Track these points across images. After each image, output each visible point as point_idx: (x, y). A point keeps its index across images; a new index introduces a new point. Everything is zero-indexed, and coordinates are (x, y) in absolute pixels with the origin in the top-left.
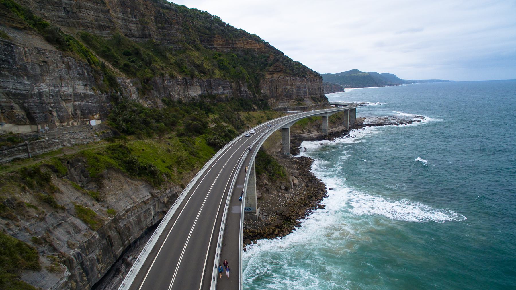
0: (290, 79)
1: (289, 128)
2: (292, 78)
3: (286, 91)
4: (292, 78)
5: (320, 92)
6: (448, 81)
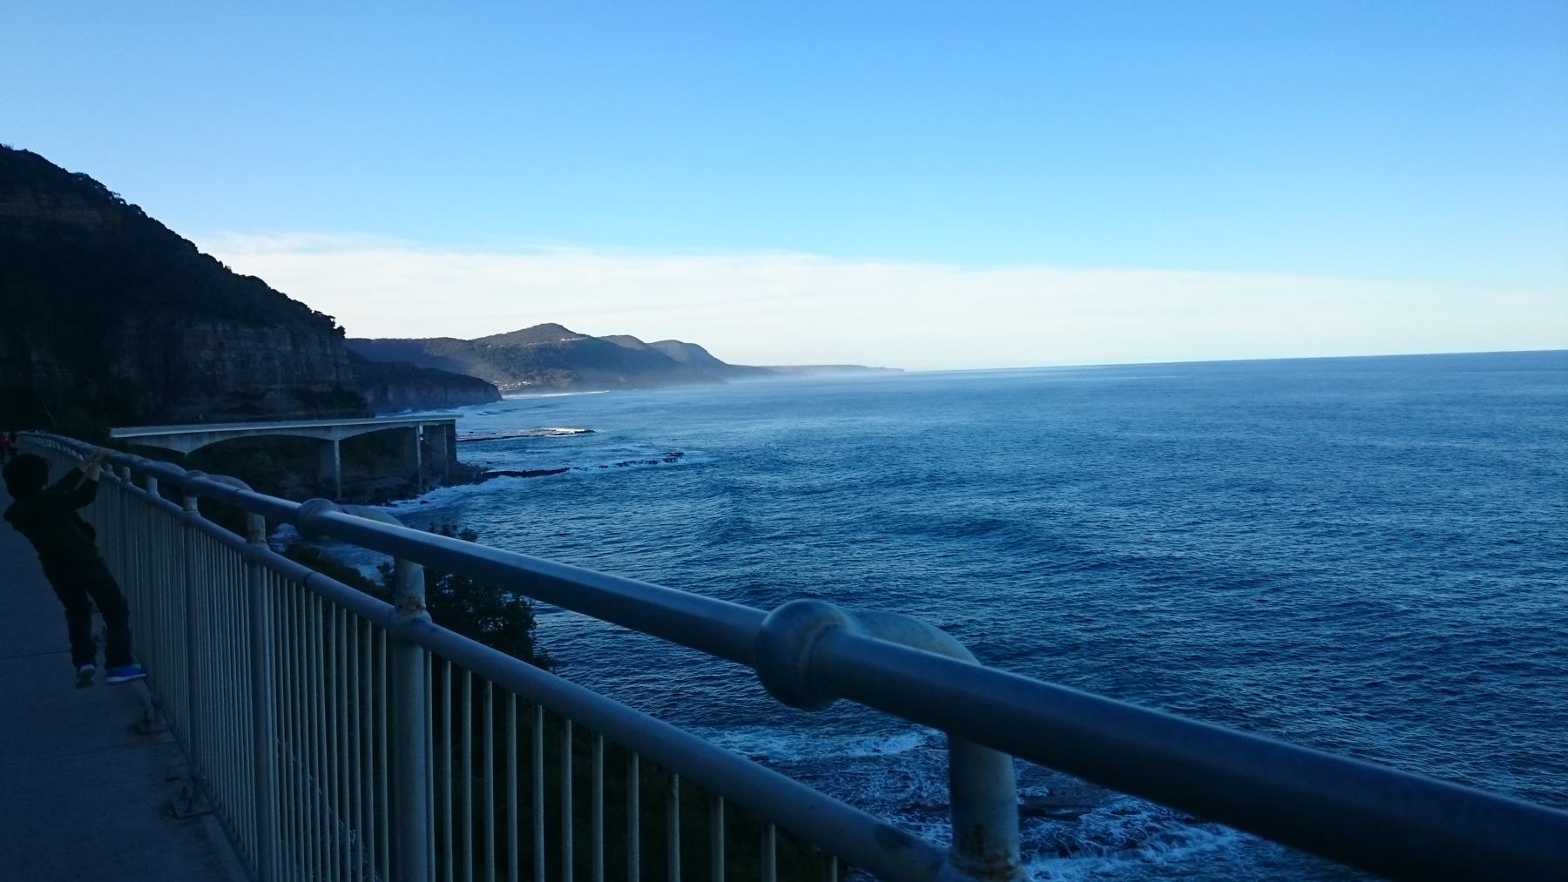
3: (201, 366)
6: (882, 369)
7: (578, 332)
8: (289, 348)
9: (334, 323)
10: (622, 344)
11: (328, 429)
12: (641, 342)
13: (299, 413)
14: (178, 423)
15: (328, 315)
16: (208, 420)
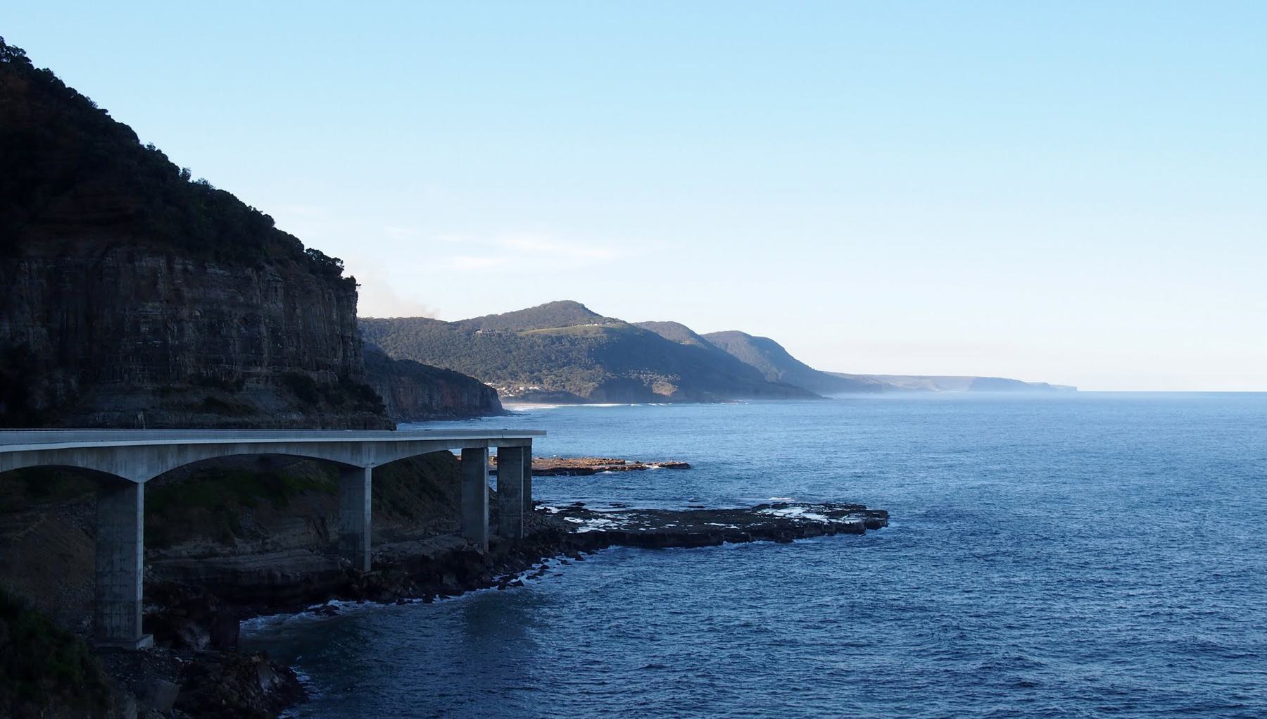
0: (170, 269)
1: (141, 482)
2: (178, 260)
3: (144, 329)
4: (178, 260)
5: (338, 361)
6: (1045, 386)
9: (341, 269)
10: (665, 335)
11: (357, 446)
12: (692, 334)
13: (295, 417)
14: (103, 426)
15: (332, 257)
16: (153, 423)
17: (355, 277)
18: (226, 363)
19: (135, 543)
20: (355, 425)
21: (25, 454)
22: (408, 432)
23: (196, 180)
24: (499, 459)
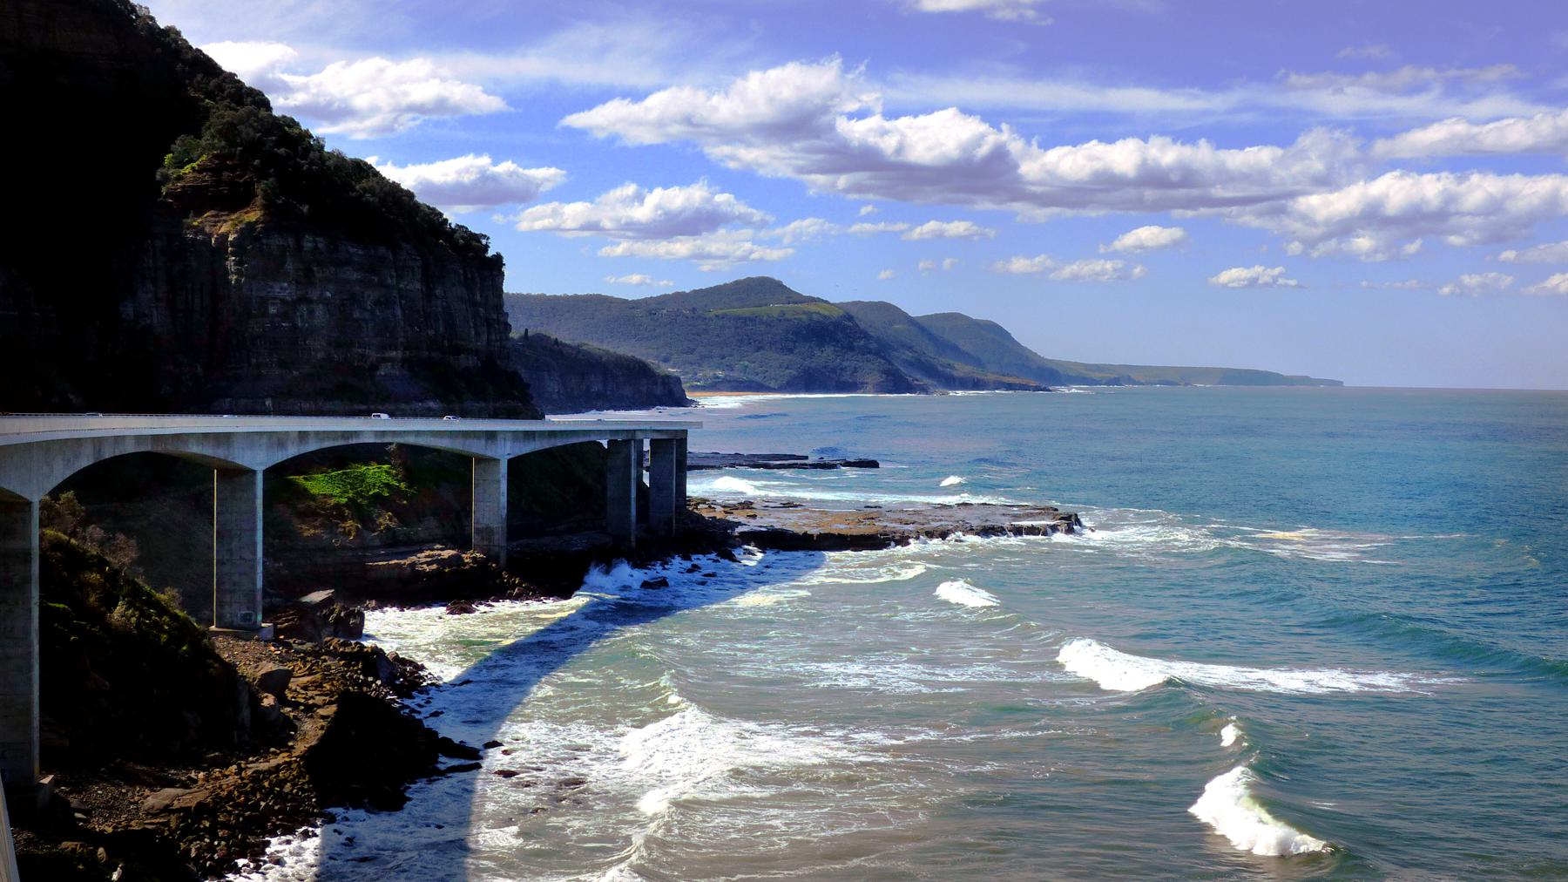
3: (272, 310)
7: (832, 302)
8: (418, 286)
9: (486, 247)
11: (491, 436)
17: (502, 254)
18: (360, 347)
19: (254, 530)
20: (495, 415)
21: (303, 436)
22: (557, 421)
23: (329, 151)
24: (653, 453)
